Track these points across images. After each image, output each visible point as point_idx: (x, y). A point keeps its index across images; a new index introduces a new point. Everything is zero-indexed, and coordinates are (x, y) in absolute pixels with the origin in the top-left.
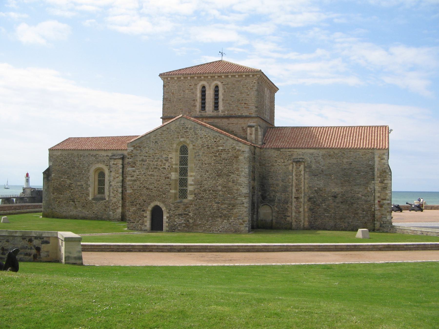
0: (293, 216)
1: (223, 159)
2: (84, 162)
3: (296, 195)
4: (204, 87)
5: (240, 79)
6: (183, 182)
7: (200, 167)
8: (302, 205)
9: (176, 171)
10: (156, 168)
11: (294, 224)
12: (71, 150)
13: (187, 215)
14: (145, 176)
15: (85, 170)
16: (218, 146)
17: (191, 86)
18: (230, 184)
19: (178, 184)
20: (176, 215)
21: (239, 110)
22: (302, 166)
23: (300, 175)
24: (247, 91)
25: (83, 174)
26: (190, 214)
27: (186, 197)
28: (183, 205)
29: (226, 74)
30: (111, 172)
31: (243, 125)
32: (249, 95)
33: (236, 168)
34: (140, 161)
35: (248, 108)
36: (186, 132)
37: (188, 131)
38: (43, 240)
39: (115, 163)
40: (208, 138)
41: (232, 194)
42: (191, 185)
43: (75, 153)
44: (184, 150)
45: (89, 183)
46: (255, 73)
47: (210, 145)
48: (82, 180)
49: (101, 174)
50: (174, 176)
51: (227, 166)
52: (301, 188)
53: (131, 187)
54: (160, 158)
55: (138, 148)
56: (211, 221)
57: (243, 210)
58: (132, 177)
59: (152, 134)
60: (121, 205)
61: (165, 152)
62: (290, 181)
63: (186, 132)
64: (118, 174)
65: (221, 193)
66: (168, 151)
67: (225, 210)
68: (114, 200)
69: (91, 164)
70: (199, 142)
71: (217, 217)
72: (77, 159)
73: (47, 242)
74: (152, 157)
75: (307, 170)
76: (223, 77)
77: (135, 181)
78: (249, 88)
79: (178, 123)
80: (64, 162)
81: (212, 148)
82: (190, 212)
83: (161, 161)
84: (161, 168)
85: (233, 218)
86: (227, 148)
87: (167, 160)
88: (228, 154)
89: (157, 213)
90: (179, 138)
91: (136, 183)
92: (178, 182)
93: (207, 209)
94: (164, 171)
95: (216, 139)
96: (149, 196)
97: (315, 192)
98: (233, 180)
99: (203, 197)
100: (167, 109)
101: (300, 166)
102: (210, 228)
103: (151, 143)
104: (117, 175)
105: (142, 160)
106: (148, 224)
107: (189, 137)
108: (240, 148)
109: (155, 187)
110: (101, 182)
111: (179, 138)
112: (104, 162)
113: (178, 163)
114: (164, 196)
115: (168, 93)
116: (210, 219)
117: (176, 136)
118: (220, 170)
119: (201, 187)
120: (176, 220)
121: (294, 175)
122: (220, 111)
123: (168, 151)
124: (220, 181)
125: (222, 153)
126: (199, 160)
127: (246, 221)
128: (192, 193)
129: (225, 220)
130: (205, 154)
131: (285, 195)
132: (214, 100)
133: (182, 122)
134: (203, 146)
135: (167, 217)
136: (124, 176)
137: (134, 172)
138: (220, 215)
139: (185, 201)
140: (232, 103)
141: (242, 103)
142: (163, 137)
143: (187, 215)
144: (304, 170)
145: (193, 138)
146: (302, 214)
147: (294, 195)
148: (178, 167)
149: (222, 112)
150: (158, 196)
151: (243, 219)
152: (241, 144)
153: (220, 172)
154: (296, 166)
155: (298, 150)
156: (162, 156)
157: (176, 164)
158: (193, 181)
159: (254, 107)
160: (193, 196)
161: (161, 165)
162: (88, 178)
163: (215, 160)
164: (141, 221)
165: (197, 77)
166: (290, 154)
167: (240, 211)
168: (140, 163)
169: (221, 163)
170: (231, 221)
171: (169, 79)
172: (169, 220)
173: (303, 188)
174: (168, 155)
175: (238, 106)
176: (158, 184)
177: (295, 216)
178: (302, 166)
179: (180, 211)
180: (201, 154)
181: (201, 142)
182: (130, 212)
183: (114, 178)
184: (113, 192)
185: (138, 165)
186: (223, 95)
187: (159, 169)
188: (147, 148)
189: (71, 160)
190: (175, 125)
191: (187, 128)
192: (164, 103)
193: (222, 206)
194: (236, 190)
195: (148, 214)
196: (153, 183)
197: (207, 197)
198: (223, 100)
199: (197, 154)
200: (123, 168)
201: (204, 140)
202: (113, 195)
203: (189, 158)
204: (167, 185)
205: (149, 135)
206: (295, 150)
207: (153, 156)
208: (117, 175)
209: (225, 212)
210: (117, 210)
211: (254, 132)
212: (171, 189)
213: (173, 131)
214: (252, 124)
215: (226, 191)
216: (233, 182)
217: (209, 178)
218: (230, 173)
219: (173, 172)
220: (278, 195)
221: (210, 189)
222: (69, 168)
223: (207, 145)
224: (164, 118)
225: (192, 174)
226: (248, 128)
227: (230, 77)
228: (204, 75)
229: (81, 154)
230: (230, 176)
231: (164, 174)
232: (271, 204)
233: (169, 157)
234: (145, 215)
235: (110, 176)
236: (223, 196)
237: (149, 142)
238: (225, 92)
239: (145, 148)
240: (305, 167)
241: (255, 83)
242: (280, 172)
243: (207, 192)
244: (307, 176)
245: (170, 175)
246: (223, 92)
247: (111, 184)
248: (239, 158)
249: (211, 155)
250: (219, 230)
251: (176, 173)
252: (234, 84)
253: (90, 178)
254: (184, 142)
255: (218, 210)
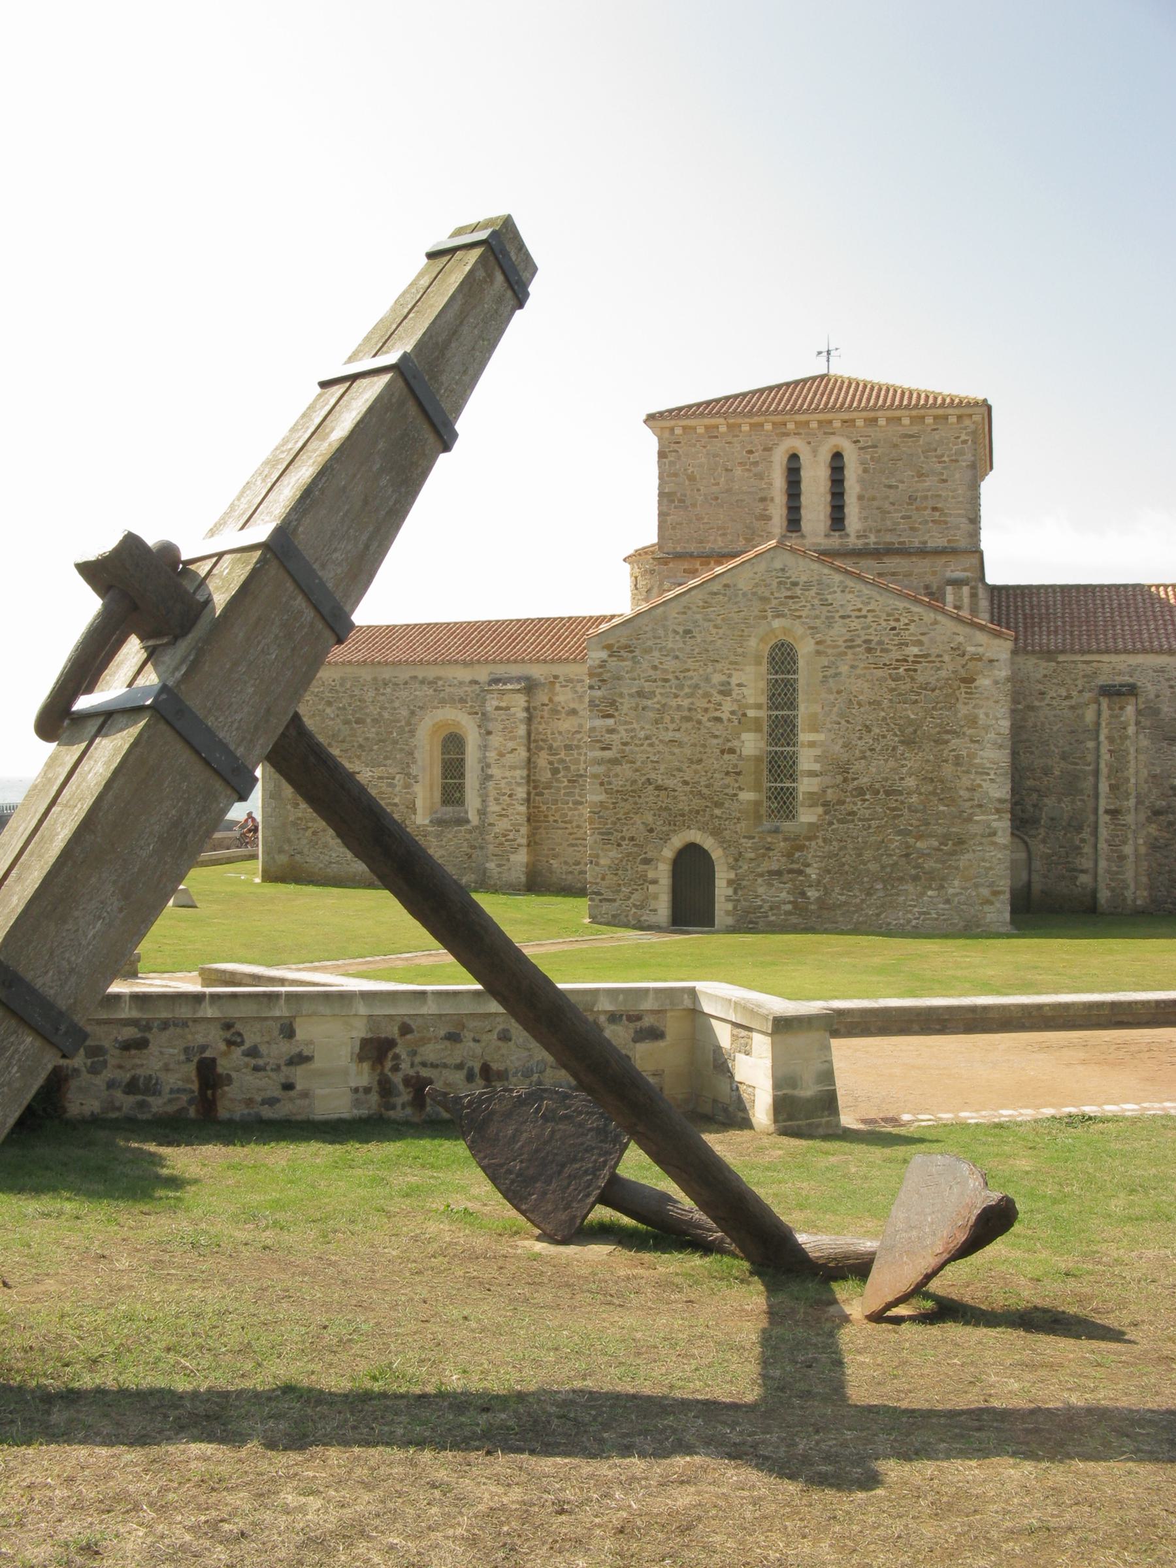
0: (1100, 871)
1: (921, 688)
2: (397, 704)
3: (1108, 803)
4: (794, 457)
5: (915, 429)
6: (780, 764)
7: (841, 715)
8: (1130, 836)
9: (758, 730)
10: (688, 719)
11: (1104, 895)
12: (386, 663)
13: (800, 872)
14: (651, 745)
15: (401, 731)
16: (903, 644)
17: (750, 452)
18: (948, 770)
19: (765, 773)
20: (761, 875)
21: (912, 529)
22: (1130, 710)
23: (1124, 738)
24: (938, 467)
25: (395, 742)
26: (808, 870)
27: (791, 815)
28: (785, 840)
29: (872, 414)
30: (489, 733)
31: (929, 579)
32: (945, 481)
33: (966, 717)
34: (631, 696)
35: (946, 523)
36: (792, 597)
37: (799, 592)
38: (639, 1024)
39: (503, 704)
40: (870, 619)
41: (952, 801)
42: (812, 774)
43: (366, 674)
44: (782, 659)
45: (414, 770)
46: (969, 411)
47: (876, 639)
48: (389, 762)
49: (453, 744)
50: (751, 744)
51: (934, 708)
52: (1127, 780)
53: (602, 784)
54: (702, 684)
55: (623, 653)
56: (881, 894)
57: (993, 857)
58: (603, 749)
59: (673, 604)
60: (524, 841)
61: (719, 666)
62: (1090, 758)
63: (792, 597)
64: (513, 739)
65: (914, 799)
66: (731, 663)
67: (928, 855)
68: (503, 825)
69: (421, 708)
70: (839, 631)
71: (901, 879)
72: (371, 694)
73: (655, 1034)
74: (674, 682)
75: (1146, 722)
76: (860, 423)
77: (615, 762)
78: (946, 459)
79: (762, 567)
80: (329, 704)
81: (882, 650)
82: (808, 865)
83: (707, 695)
84: (705, 719)
85: (956, 883)
86: (934, 651)
87: (726, 693)
88: (939, 669)
89: (692, 870)
90: (765, 617)
91: (618, 769)
92: (765, 766)
93: (868, 854)
94: (718, 729)
95: (898, 620)
96: (664, 814)
97: (1171, 792)
98: (957, 757)
99: (852, 813)
100: (674, 528)
101: (1122, 708)
102: (878, 915)
103: (671, 635)
104: (511, 745)
105: (640, 694)
106: (663, 907)
107: (803, 614)
108: (981, 650)
109: (686, 783)
110: (453, 768)
111: (765, 617)
112: (462, 700)
113: (763, 699)
114: (717, 812)
115: (676, 475)
116: (879, 886)
117: (756, 613)
118: (911, 723)
119: (845, 780)
120: (761, 890)
121: (1102, 738)
122: (853, 535)
123: (731, 663)
124: (913, 761)
125: (918, 667)
126: (839, 692)
127: (1003, 892)
128: (814, 799)
129: (930, 888)
130: (859, 671)
131: (1073, 802)
132: (829, 498)
133: (778, 565)
134: (850, 644)
135: (730, 883)
136: (533, 745)
137: (611, 731)
138: (913, 872)
139: (787, 826)
140: (892, 508)
141: (925, 508)
142: (713, 616)
143: (800, 872)
144: (1137, 723)
145: (817, 617)
146: (1130, 865)
147: (1103, 804)
148: (763, 714)
149: (858, 537)
150: (698, 812)
151: (991, 885)
152: (981, 637)
153: (911, 730)
154: (1110, 708)
155: (1113, 658)
156: (707, 680)
157: (758, 706)
158: (816, 761)
159: (964, 520)
160: (820, 810)
161: (706, 710)
162: (411, 754)
163: (892, 690)
164: (636, 897)
165: (774, 424)
166: (1089, 669)
167: (984, 860)
168: (633, 702)
169: (916, 702)
170: (951, 891)
171: (678, 431)
172: (735, 892)
173: (1133, 781)
174: (730, 676)
175: (909, 517)
176: (696, 772)
177: (1108, 871)
178: (1130, 710)
179: (776, 862)
180: (844, 669)
181: (844, 630)
182: (597, 864)
183: (501, 755)
184: (496, 799)
185: (625, 709)
186: (861, 481)
187: (699, 722)
188: (656, 654)
189: (352, 696)
190: (751, 575)
191: (795, 584)
192: (665, 509)
193: (918, 844)
194: (967, 789)
195: (662, 873)
196: (679, 770)
197: (868, 812)
198: (860, 498)
199: (832, 671)
200: (529, 720)
201: (855, 624)
202: (497, 808)
203: (802, 684)
204: (727, 773)
205: (661, 609)
206: (1105, 658)
207: (677, 678)
208: (511, 745)
209: (930, 864)
210: (513, 857)
211: (966, 601)
212: (741, 789)
213: (744, 595)
214: (958, 574)
215: (934, 793)
216: (957, 764)
217: (872, 750)
218: (948, 732)
219: (749, 730)
220: (1050, 801)
221: (877, 786)
222: (347, 722)
223: (865, 642)
224: (661, 562)
225: (812, 737)
226: (949, 589)
227: (882, 422)
228: (798, 418)
229: (387, 676)
230: (947, 742)
231: (716, 737)
232: (1026, 834)
233: (734, 681)
234: (651, 875)
235: (484, 747)
236: (924, 811)
237: (661, 632)
238: (865, 471)
239: (648, 651)
240: (1139, 712)
241: (965, 442)
242: (1055, 728)
243: (867, 797)
244: (1145, 742)
245: (735, 743)
246: (860, 472)
247: (490, 772)
248: (977, 683)
249: (879, 673)
250: (909, 921)
251: (759, 735)
252: (895, 446)
253: (416, 755)
254: (786, 631)
255: (907, 855)
